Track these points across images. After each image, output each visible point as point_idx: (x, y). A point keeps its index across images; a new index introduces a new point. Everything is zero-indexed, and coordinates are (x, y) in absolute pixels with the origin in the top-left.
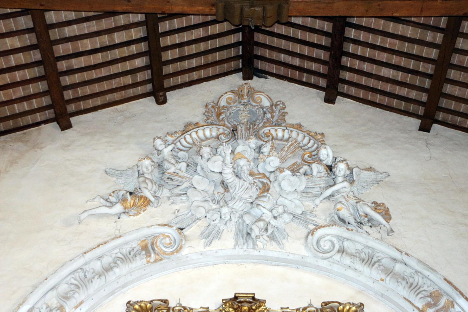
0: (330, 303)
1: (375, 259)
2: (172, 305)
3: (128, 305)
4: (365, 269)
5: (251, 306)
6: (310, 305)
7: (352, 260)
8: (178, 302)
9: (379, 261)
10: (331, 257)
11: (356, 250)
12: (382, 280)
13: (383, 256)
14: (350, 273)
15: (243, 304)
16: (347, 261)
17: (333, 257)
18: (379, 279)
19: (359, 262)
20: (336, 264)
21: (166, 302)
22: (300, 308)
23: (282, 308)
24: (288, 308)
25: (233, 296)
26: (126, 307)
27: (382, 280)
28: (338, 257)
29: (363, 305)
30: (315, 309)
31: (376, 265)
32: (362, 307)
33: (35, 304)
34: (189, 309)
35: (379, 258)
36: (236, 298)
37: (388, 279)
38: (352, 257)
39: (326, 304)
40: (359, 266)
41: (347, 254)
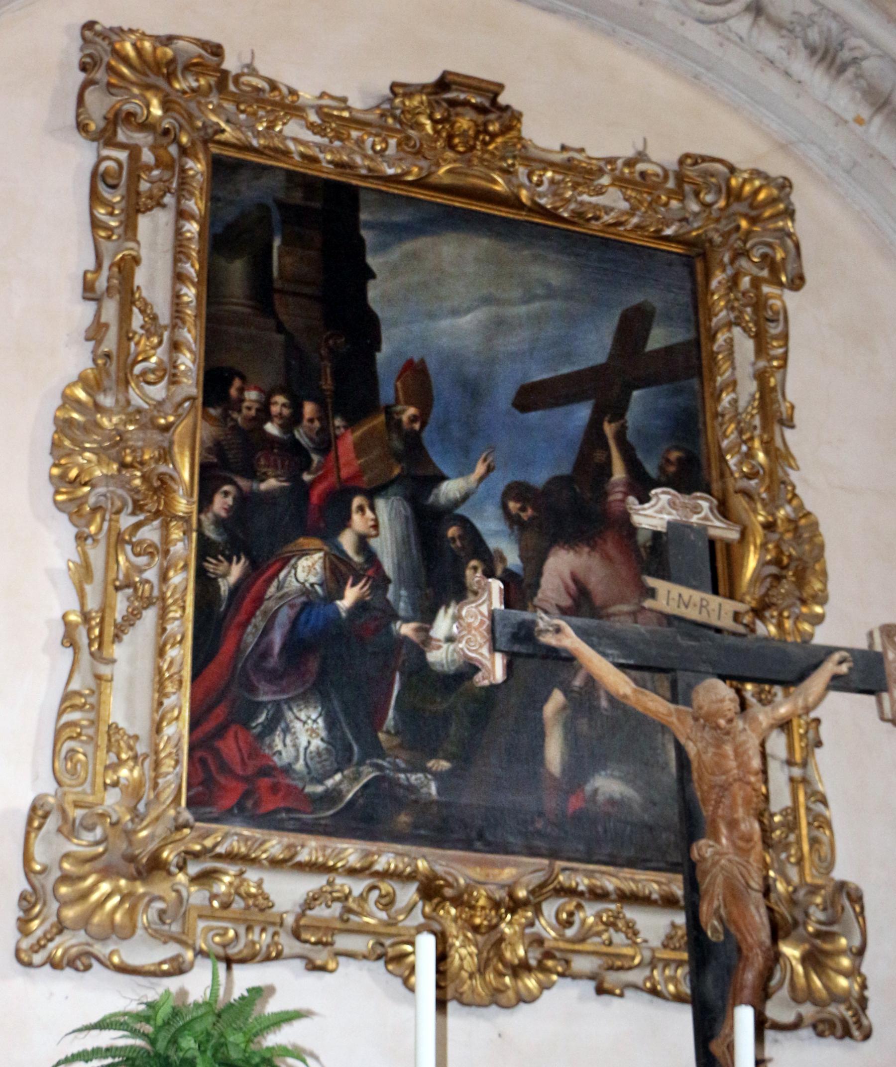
0: (704, 159)
1: (845, 55)
2: (231, 64)
3: (88, 34)
4: (817, 79)
5: (485, 124)
6: (641, 157)
7: (784, 42)
8: (247, 61)
9: (855, 61)
10: (724, 20)
11: (795, 13)
12: (859, 121)
13: (868, 49)
14: (774, 82)
15: (459, 109)
16: (771, 43)
17: (731, 22)
18: (849, 116)
19: (803, 53)
20: (735, 43)
21: (217, 51)
22: (618, 158)
23: (564, 148)
24: (582, 150)
25: (431, 76)
26: (80, 42)
27: (859, 121)
28: (742, 25)
29: (791, 186)
30: (659, 171)
31: (850, 73)
32: (788, 190)
33: (82, 605)
34: (285, 91)
35: (857, 54)
36: (444, 83)
37: (878, 120)
38: (784, 32)
39: (698, 159)
40: (800, 66)
41: (770, 20)
